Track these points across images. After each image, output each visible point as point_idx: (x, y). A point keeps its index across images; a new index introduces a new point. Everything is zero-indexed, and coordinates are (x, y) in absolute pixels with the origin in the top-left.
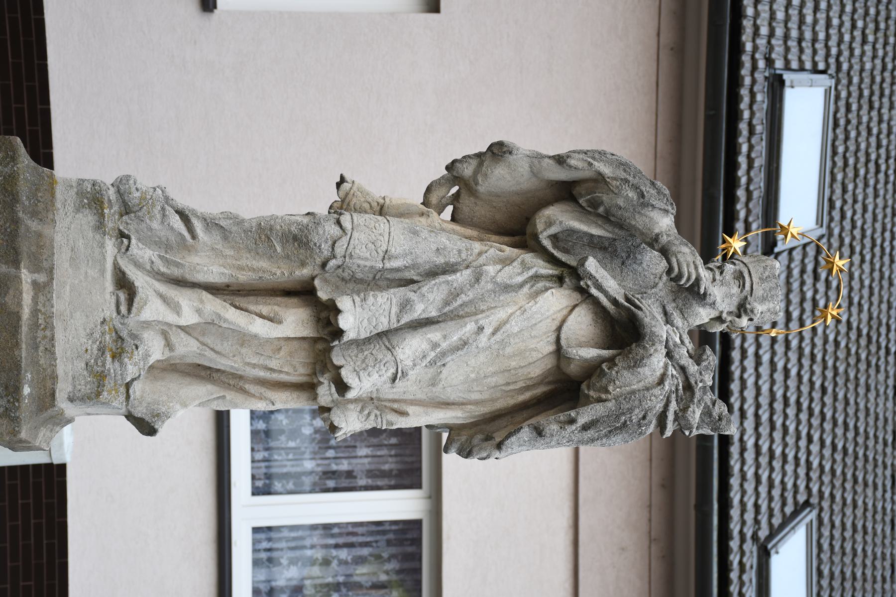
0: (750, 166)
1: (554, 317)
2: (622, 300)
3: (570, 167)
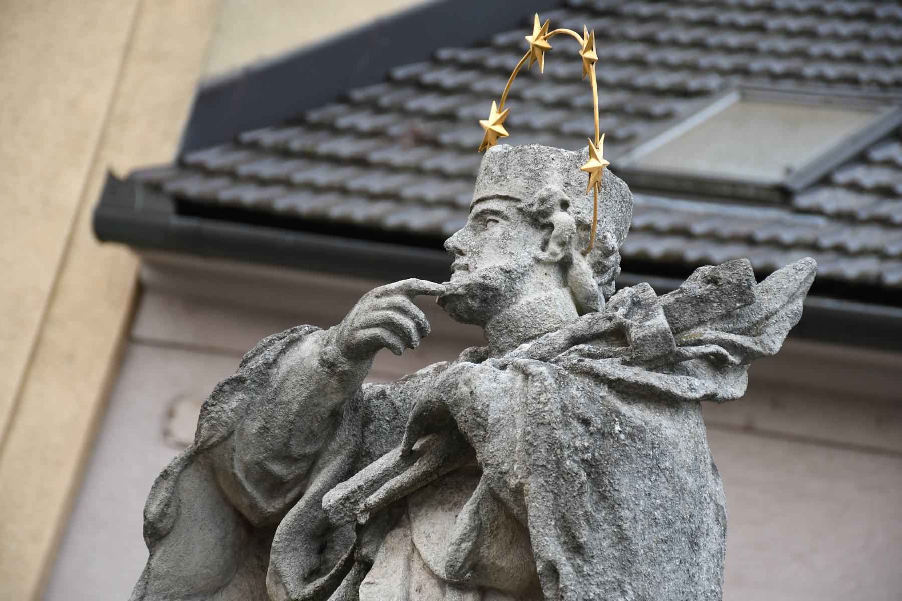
1: (414, 587)
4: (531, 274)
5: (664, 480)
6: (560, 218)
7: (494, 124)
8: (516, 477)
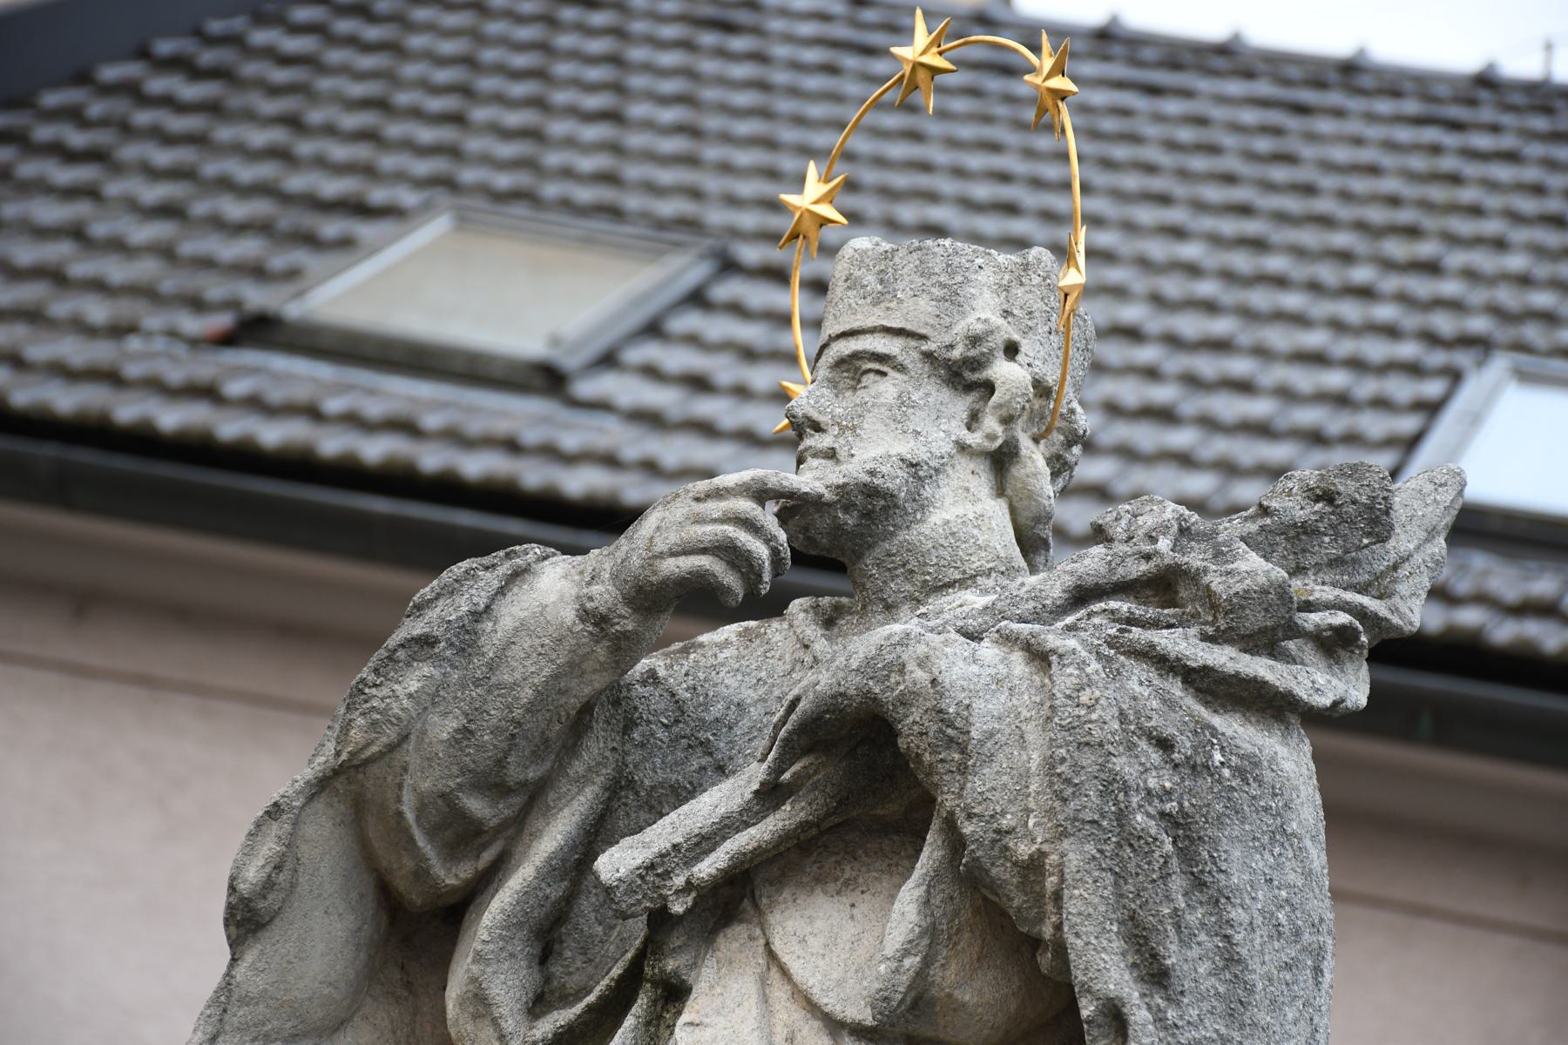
4: (948, 468)
5: (1290, 855)
6: (1006, 373)
7: (816, 202)
8: (1033, 841)
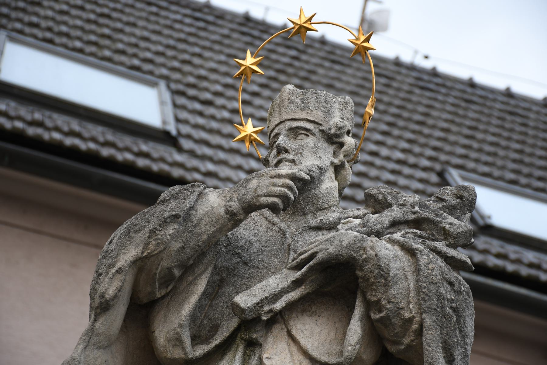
0: (78, 135)
2: (298, 274)
3: (116, 296)
8: (411, 313)
